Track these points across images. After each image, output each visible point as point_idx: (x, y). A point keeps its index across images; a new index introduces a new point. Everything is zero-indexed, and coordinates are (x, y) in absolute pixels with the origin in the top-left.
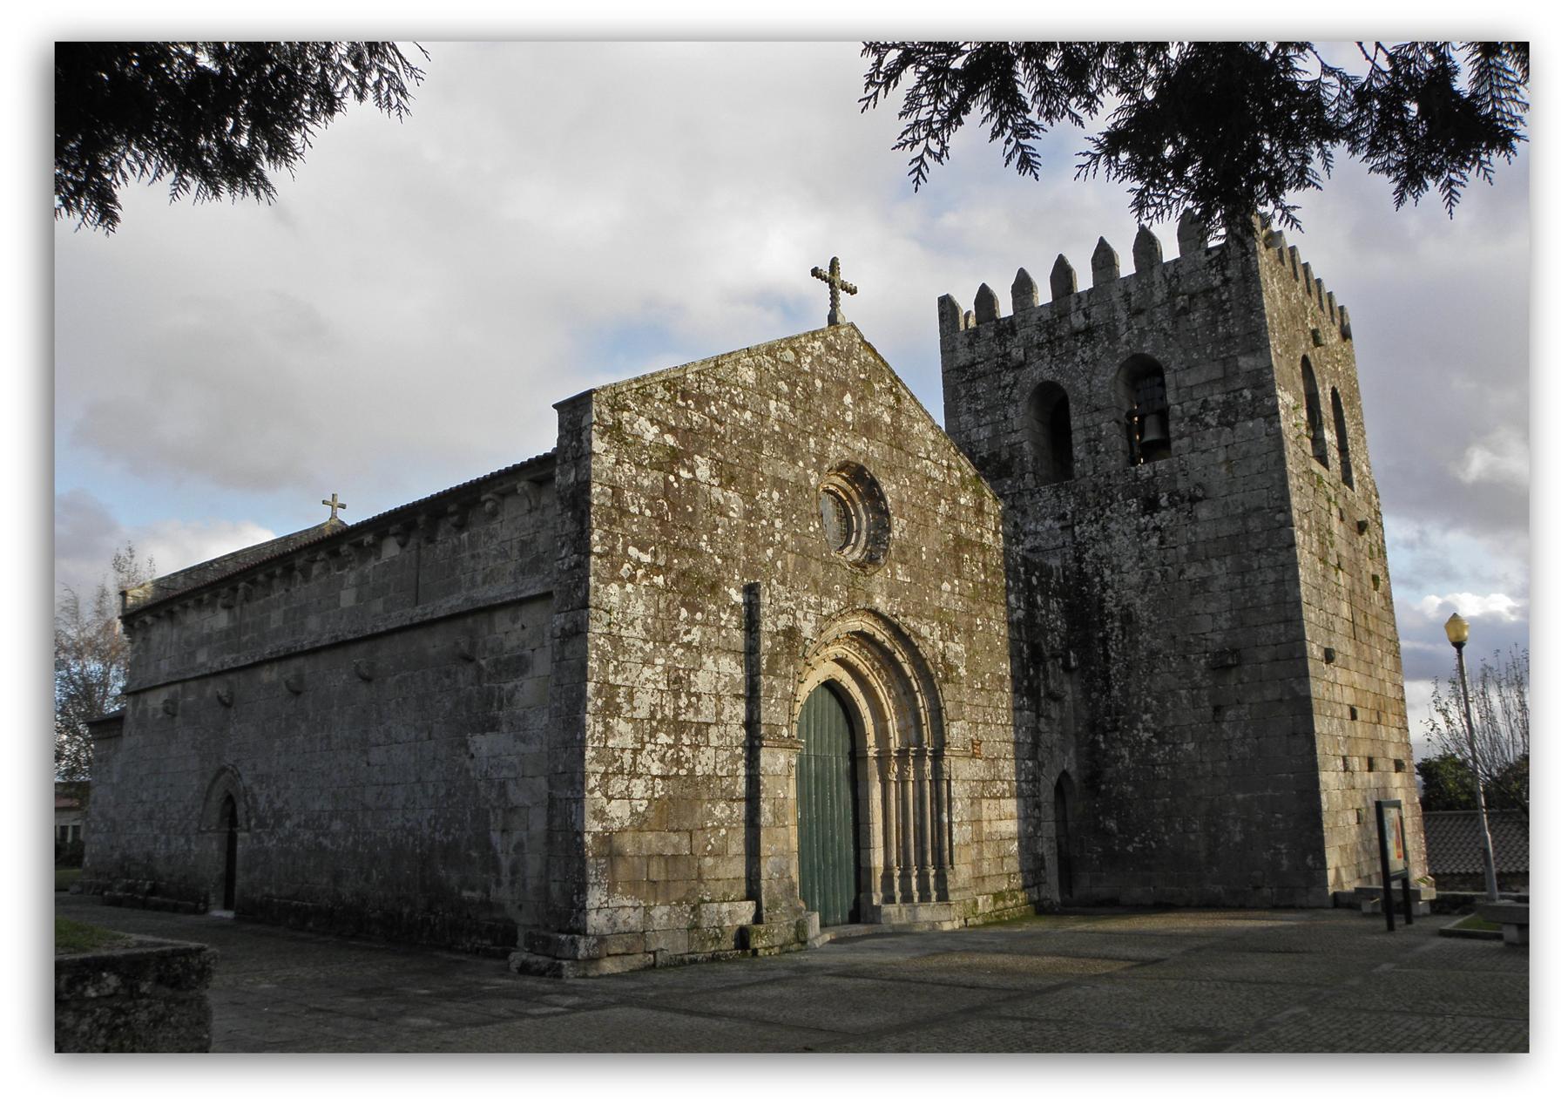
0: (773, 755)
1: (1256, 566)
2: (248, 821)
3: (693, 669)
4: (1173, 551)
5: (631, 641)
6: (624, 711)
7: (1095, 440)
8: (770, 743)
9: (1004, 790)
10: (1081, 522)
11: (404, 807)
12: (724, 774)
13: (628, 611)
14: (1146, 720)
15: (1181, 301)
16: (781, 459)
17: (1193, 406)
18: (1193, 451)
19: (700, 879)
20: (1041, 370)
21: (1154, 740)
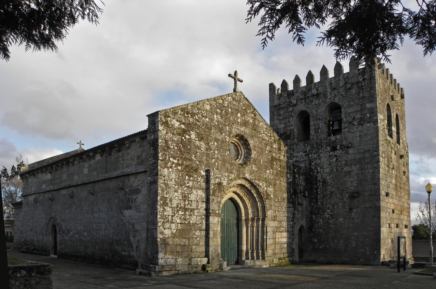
0: (213, 218)
1: (366, 168)
2: (60, 232)
4: (340, 163)
5: (171, 185)
6: (169, 205)
7: (317, 129)
9: (283, 230)
10: (311, 153)
11: (105, 229)
16: (217, 133)
17: (350, 119)
18: (349, 133)
19: (191, 251)
20: (301, 107)
21: (330, 217)
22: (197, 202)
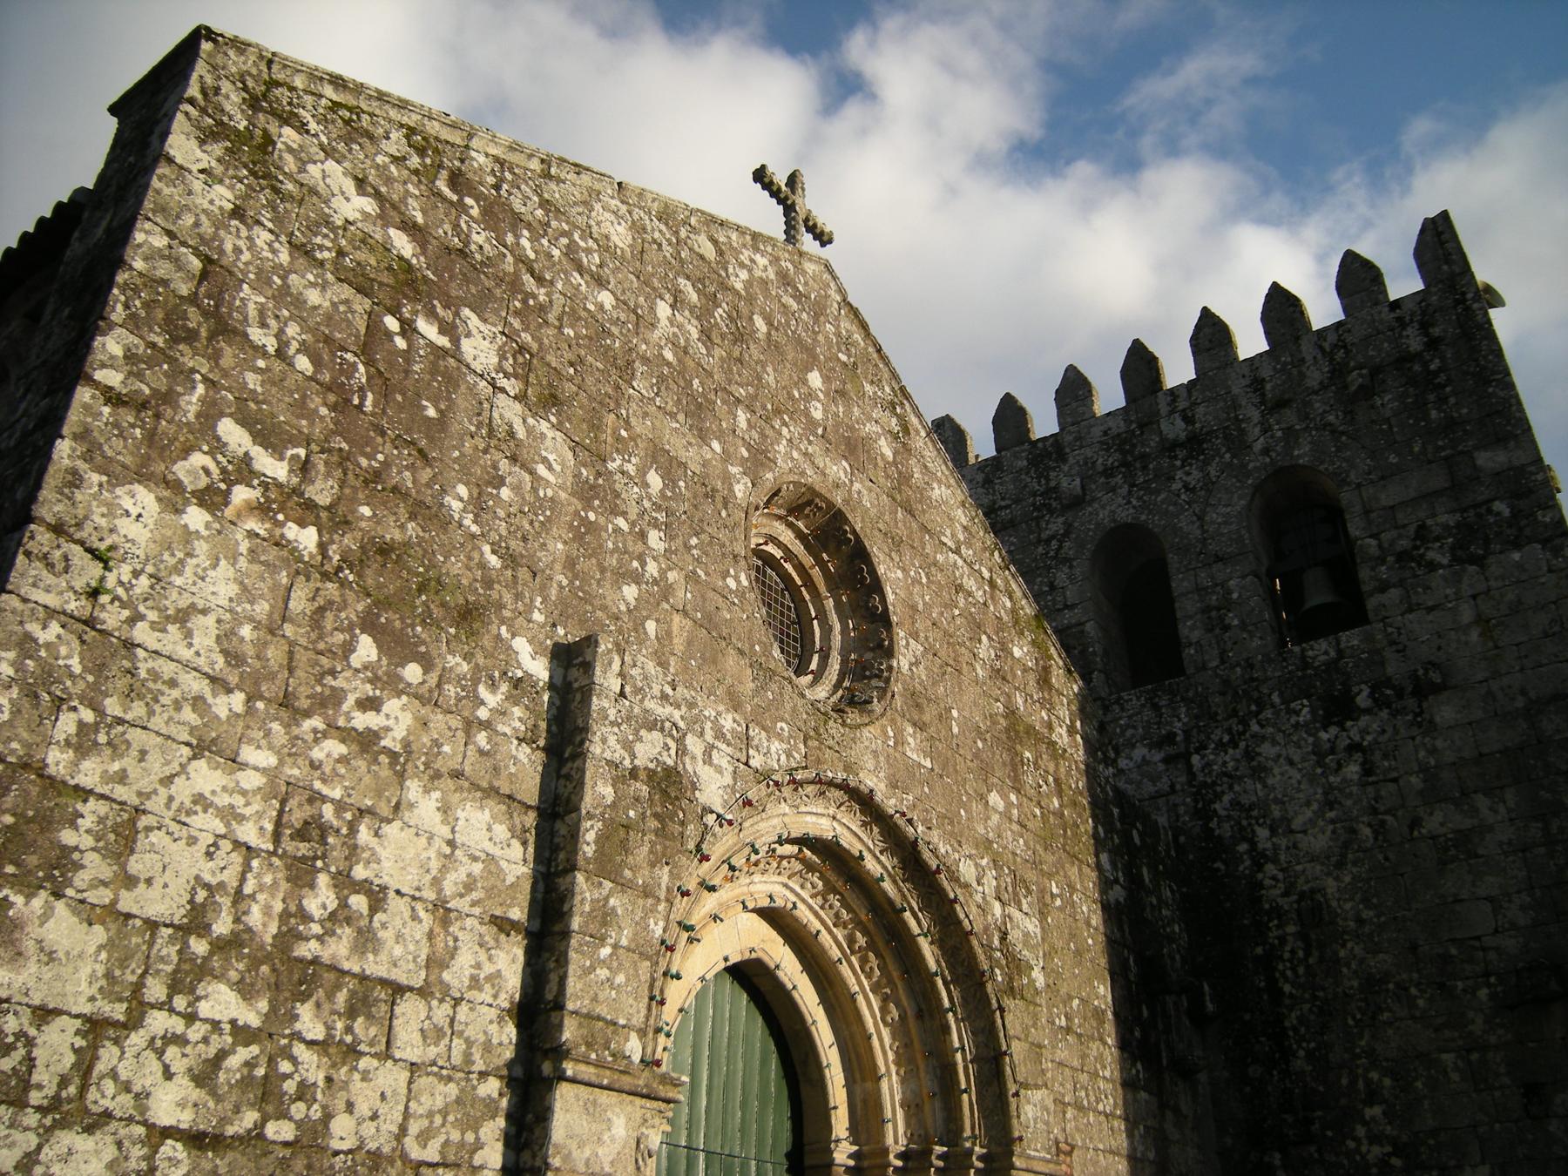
0: (590, 1109)
3: (370, 812)
4: (1392, 787)
5: (168, 669)
6: (81, 878)
7: (1218, 609)
8: (587, 1072)
10: (1202, 748)
12: (432, 1153)
13: (178, 581)
14: (1373, 1118)
15: (1355, 379)
16: (673, 416)
17: (1400, 536)
18: (1410, 610)
22: (443, 912)
